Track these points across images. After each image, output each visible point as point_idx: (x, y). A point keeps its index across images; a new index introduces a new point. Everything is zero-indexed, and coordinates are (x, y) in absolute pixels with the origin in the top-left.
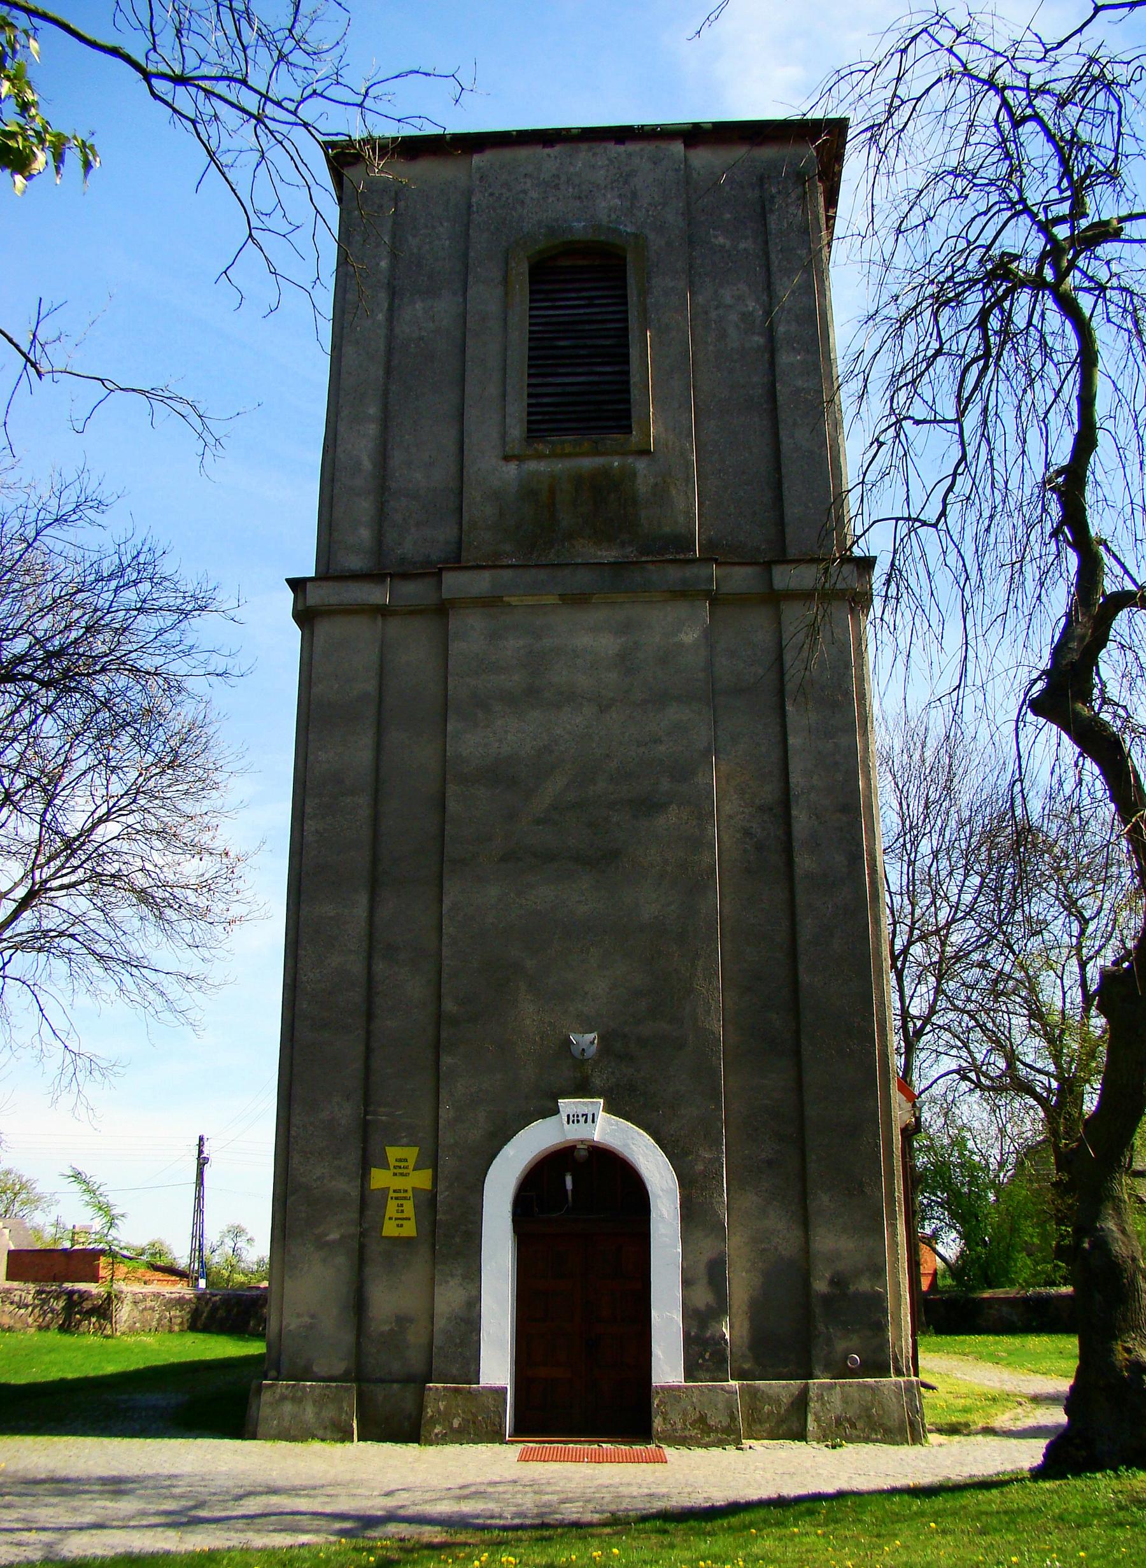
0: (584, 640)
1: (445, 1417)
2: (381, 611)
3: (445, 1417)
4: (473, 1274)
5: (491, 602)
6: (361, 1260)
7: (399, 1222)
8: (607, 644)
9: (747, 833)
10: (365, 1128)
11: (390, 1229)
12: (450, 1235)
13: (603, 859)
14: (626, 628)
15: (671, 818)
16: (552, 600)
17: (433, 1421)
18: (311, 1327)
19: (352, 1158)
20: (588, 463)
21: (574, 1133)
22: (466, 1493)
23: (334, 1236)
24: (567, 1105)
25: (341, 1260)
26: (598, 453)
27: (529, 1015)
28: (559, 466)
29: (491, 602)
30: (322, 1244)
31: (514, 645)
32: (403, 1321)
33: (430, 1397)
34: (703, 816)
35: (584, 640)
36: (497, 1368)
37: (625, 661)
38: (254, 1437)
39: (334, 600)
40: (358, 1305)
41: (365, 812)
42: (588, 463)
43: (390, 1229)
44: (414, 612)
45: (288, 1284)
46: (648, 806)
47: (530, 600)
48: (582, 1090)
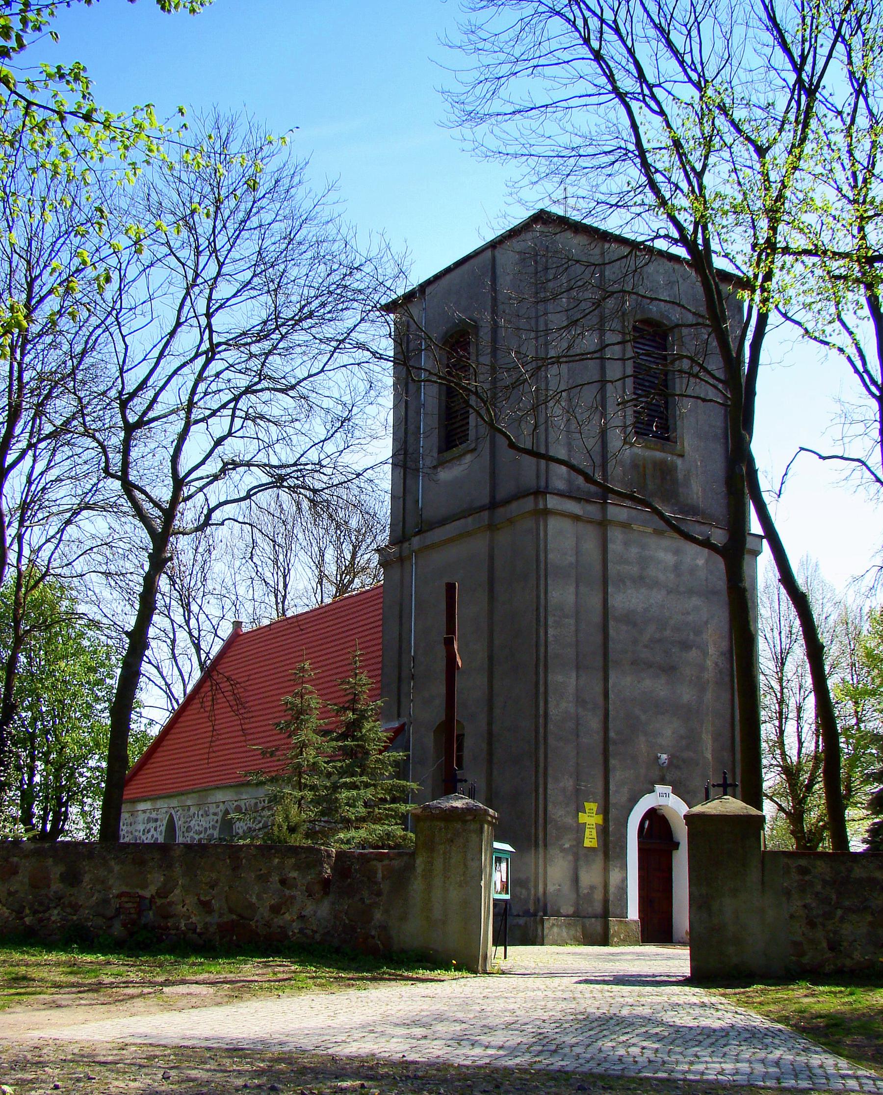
0: (661, 555)
1: (617, 934)
2: (576, 518)
3: (617, 934)
4: (624, 867)
5: (625, 526)
6: (576, 859)
7: (590, 840)
8: (669, 559)
9: (716, 664)
10: (577, 791)
11: (587, 843)
12: (611, 845)
13: (669, 670)
14: (677, 552)
15: (694, 653)
16: (650, 530)
17: (613, 936)
18: (559, 890)
19: (572, 807)
20: (659, 455)
21: (662, 801)
22: (241, 990)
23: (567, 846)
24: (659, 788)
25: (570, 858)
26: (663, 451)
27: (642, 745)
28: (647, 453)
29: (625, 526)
30: (563, 850)
31: (634, 550)
32: (592, 888)
33: (611, 924)
34: (705, 653)
35: (661, 555)
36: (633, 913)
37: (676, 568)
38: (542, 944)
39: (560, 507)
40: (576, 880)
41: (573, 628)
42: (659, 455)
43: (587, 843)
44: (590, 522)
45: (549, 869)
46: (686, 646)
47: (641, 529)
48: (663, 782)
